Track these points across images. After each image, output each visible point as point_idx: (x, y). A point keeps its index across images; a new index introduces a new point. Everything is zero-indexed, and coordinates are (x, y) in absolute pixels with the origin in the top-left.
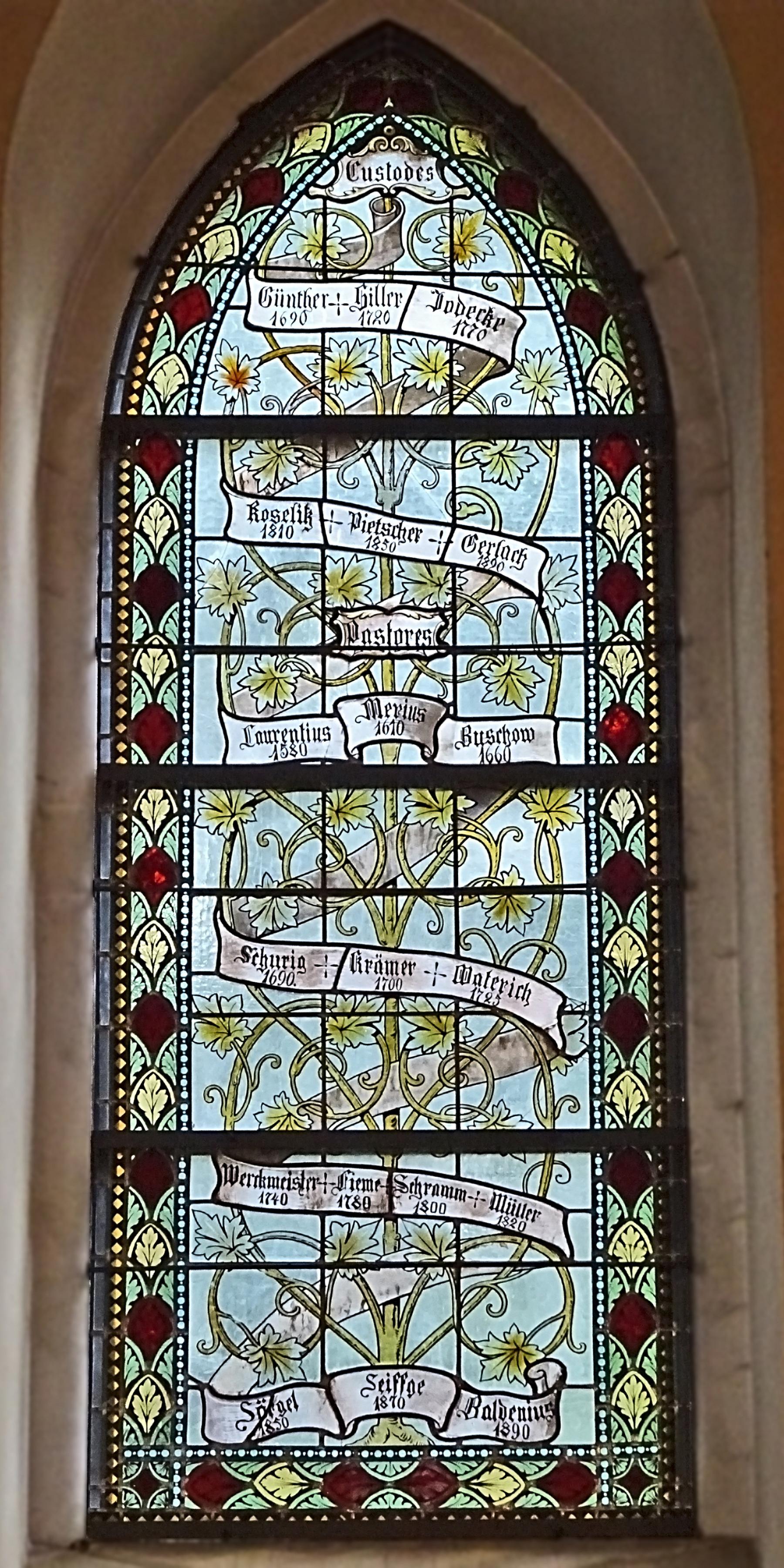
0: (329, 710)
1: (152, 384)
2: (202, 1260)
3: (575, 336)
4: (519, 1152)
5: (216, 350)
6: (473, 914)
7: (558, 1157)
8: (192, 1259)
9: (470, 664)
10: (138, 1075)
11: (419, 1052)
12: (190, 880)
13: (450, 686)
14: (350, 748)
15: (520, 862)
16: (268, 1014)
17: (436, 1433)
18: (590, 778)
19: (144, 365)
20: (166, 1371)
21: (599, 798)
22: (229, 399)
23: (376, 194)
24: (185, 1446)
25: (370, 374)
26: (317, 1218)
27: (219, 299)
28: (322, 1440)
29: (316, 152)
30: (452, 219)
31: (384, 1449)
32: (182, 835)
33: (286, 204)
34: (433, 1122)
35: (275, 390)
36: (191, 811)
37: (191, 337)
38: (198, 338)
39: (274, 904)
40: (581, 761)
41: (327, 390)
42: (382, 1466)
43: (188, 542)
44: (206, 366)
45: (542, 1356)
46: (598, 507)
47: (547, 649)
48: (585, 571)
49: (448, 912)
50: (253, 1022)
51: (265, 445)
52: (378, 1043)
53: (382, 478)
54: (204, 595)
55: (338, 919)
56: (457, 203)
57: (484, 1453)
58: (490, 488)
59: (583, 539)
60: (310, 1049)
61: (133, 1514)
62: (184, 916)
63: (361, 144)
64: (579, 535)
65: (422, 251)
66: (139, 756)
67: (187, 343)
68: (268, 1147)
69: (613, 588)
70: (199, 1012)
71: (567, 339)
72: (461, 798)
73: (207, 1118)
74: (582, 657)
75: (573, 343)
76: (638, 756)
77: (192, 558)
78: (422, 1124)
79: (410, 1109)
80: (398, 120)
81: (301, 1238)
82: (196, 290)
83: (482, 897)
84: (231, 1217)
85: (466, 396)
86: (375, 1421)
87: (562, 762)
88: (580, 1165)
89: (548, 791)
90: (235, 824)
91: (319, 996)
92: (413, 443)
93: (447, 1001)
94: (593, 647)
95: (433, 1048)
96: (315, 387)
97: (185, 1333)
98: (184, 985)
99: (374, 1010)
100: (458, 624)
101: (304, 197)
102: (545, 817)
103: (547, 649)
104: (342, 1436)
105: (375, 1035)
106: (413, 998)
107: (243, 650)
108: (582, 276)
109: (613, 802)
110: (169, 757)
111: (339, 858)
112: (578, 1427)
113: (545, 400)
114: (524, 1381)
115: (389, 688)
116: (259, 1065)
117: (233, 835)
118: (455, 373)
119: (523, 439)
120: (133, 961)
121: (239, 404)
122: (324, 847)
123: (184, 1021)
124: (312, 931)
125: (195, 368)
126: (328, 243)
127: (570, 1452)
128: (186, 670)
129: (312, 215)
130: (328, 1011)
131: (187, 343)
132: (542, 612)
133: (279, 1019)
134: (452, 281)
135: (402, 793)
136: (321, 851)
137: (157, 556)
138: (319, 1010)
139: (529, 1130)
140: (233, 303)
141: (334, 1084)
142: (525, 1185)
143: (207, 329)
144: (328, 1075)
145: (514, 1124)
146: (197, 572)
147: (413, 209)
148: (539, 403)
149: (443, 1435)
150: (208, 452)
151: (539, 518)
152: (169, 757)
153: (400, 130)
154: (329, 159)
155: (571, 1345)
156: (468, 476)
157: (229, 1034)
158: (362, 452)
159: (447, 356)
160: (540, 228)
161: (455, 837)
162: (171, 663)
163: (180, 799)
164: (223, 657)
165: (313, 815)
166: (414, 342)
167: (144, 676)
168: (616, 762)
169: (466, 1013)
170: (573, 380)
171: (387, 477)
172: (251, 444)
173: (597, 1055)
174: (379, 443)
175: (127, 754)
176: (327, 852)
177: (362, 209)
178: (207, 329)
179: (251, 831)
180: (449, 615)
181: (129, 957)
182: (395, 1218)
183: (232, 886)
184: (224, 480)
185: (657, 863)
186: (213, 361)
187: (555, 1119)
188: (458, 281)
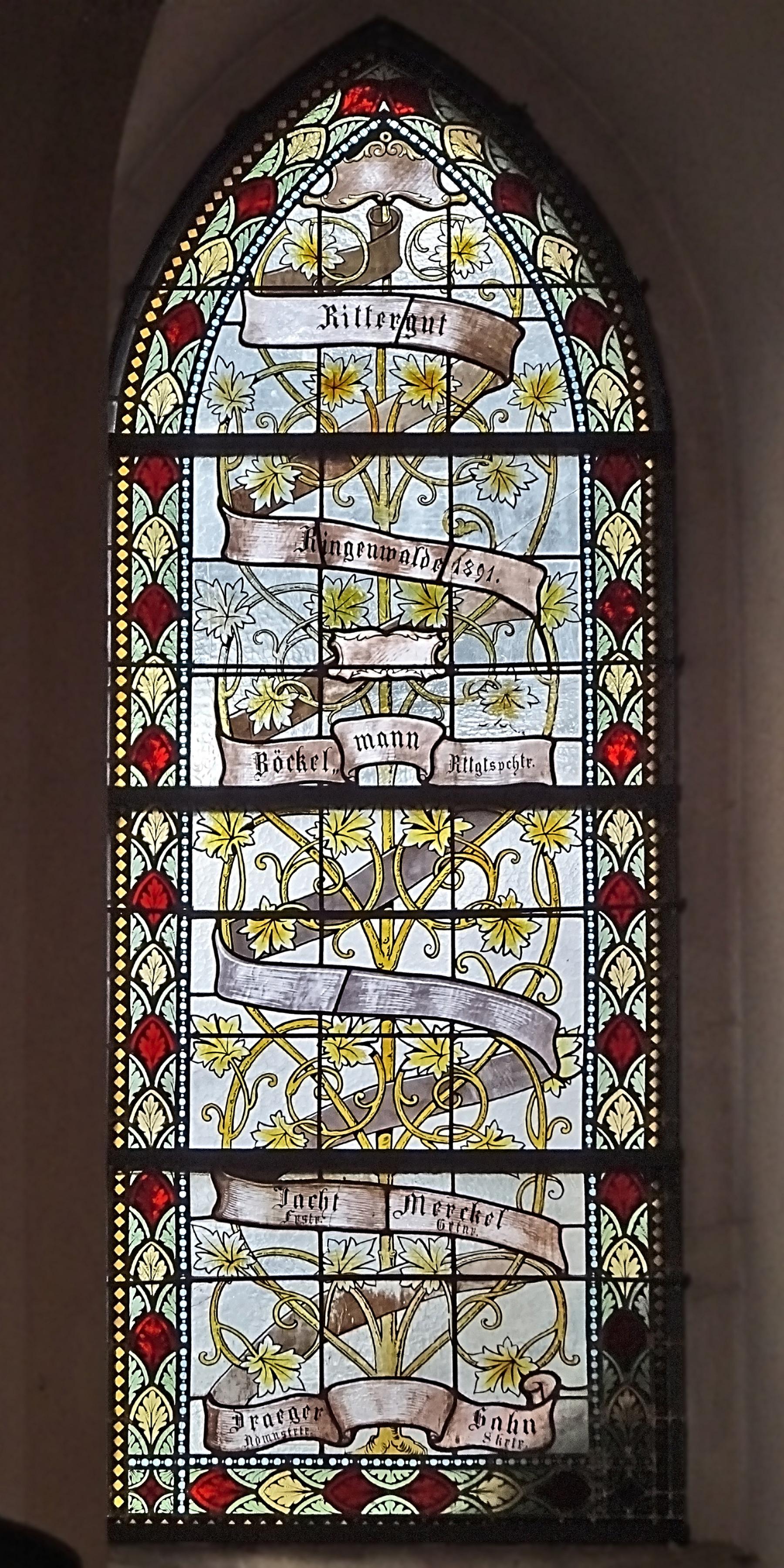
0: (326, 732)
1: (146, 404)
3: (575, 346)
5: (211, 368)
6: (469, 938)
8: (195, 1273)
10: (137, 1096)
13: (447, 708)
14: (346, 772)
15: (517, 884)
16: (267, 1035)
18: (588, 799)
22: (222, 419)
23: (371, 203)
26: (316, 1234)
27: (213, 316)
29: (310, 160)
31: (383, 1457)
32: (180, 640)
33: (280, 213)
34: (426, 1142)
35: (274, 408)
36: (189, 836)
37: (185, 356)
38: (191, 356)
40: (579, 783)
42: (381, 1473)
43: (185, 563)
44: (200, 385)
45: (534, 1368)
47: (545, 668)
48: (584, 590)
49: (445, 936)
50: (250, 1042)
52: (375, 1063)
54: (203, 619)
55: (335, 943)
57: (482, 1462)
59: (582, 557)
60: (305, 1069)
61: (140, 1518)
62: (185, 942)
63: (355, 150)
64: (578, 553)
66: (138, 778)
67: (180, 361)
68: (261, 1166)
69: (612, 607)
70: (197, 1032)
71: (566, 351)
73: (204, 1136)
74: (580, 676)
75: (572, 355)
76: (635, 777)
77: (190, 579)
78: (415, 1144)
79: (403, 1129)
80: (394, 124)
81: (297, 1253)
82: (189, 308)
83: (479, 920)
84: (230, 1233)
86: (374, 1431)
89: (546, 812)
90: (234, 847)
91: (316, 1017)
93: (442, 1024)
94: (592, 668)
95: (428, 1069)
96: (312, 848)
97: (188, 1346)
98: (183, 1006)
99: (369, 1032)
101: (298, 206)
102: (544, 840)
103: (545, 668)
105: (372, 1055)
106: (408, 1020)
108: (583, 286)
109: (145, 823)
110: (168, 779)
111: (337, 881)
114: (518, 1392)
116: (256, 1086)
117: (230, 639)
118: (452, 389)
120: (133, 984)
121: (233, 423)
122: (322, 869)
123: (183, 1041)
124: (308, 952)
125: (189, 388)
129: (308, 223)
130: (324, 1032)
131: (180, 361)
134: (449, 294)
135: (399, 815)
136: (318, 875)
138: (316, 1031)
139: (522, 1150)
140: (227, 319)
141: (330, 1102)
142: (519, 1201)
143: (201, 347)
144: (323, 1092)
145: (508, 1145)
146: (195, 595)
147: (412, 216)
148: (537, 419)
150: (204, 471)
151: (536, 541)
152: (168, 779)
153: (396, 135)
154: (324, 166)
155: (564, 1359)
156: (466, 494)
159: (444, 370)
160: (538, 233)
161: (452, 859)
163: (179, 824)
165: (311, 839)
166: (411, 358)
167: (610, 695)
168: (613, 783)
169: (460, 1035)
170: (571, 393)
174: (377, 459)
175: (126, 777)
176: (325, 874)
177: (359, 217)
178: (201, 347)
180: (446, 635)
181: (129, 836)
182: (390, 1233)
183: (230, 908)
184: (220, 498)
185: (657, 887)
186: (208, 378)
187: (547, 1140)
188: (455, 294)
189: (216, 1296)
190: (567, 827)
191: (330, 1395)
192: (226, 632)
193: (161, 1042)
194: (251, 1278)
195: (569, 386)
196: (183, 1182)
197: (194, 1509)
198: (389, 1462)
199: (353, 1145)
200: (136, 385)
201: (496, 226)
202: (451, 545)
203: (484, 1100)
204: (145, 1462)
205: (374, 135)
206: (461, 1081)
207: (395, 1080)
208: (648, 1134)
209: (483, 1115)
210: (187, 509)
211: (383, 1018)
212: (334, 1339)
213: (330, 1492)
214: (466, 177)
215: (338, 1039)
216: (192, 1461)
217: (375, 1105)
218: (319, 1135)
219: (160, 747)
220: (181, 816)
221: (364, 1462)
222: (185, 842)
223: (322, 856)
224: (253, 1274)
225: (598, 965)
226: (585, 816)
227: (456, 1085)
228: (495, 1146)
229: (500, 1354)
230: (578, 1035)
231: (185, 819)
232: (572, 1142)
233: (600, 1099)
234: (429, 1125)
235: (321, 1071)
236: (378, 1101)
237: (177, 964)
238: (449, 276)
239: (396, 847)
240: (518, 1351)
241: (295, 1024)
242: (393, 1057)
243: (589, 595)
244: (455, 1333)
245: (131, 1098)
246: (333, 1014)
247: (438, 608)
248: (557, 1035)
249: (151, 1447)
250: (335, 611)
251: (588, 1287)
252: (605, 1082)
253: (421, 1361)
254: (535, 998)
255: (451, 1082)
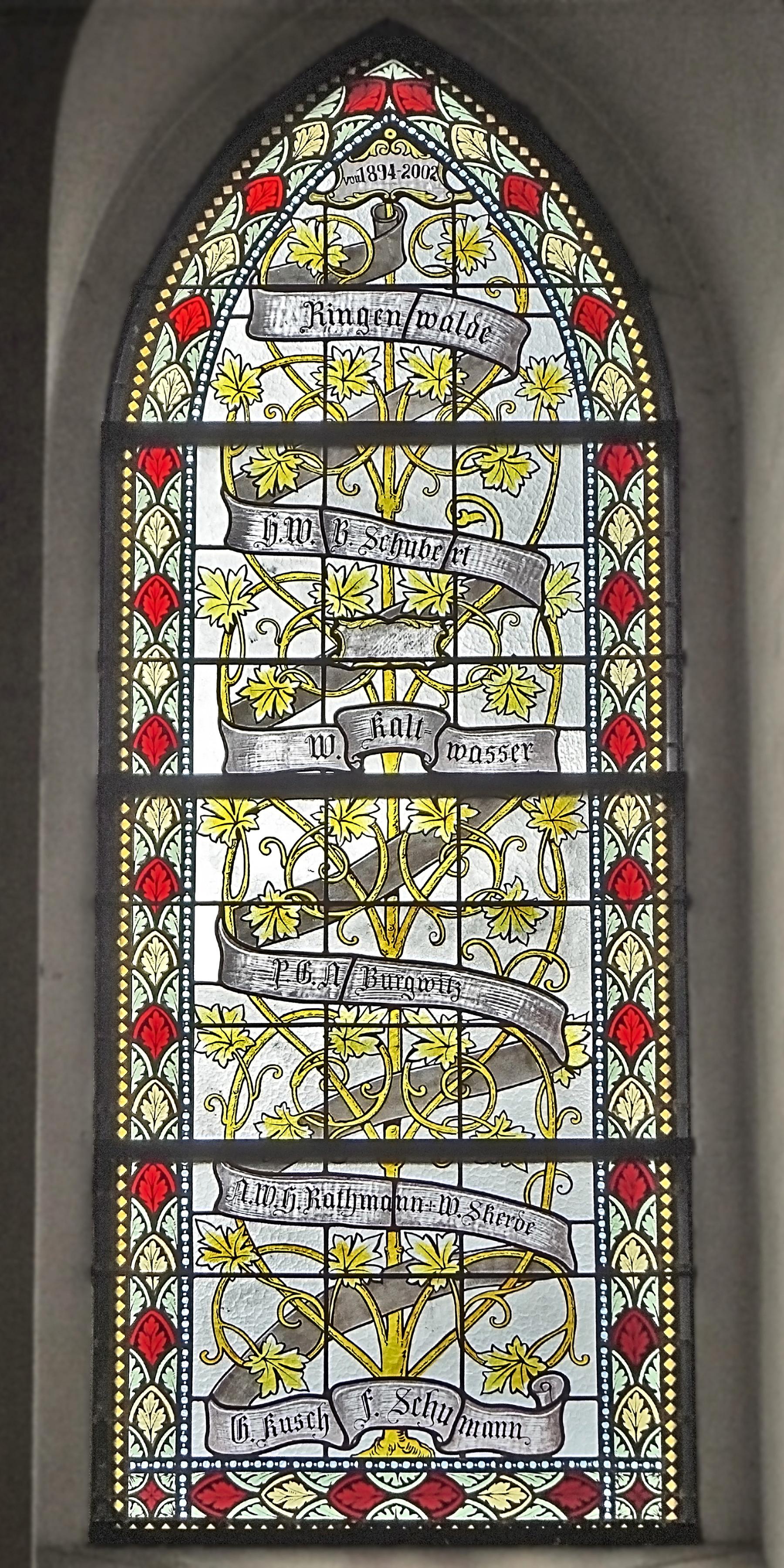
0: (330, 720)
2: (206, 1270)
4: (520, 1162)
5: (219, 360)
6: (475, 925)
7: (559, 1166)
8: (197, 1270)
9: (470, 674)
11: (422, 1063)
12: (192, 892)
17: (439, 1446)
19: (146, 375)
20: (170, 1382)
21: (602, 809)
23: (378, 200)
24: (189, 1459)
25: (373, 382)
27: (222, 306)
28: (326, 1452)
30: (454, 224)
31: (388, 1460)
36: (193, 822)
39: (276, 915)
41: (329, 398)
42: (387, 1476)
45: (543, 1368)
46: (601, 513)
48: (587, 579)
50: (255, 1032)
51: (265, 451)
53: (382, 485)
54: (206, 607)
56: (459, 208)
58: (490, 495)
59: (585, 546)
60: (312, 1061)
65: (425, 258)
66: (139, 767)
72: (464, 807)
73: (207, 1127)
78: (423, 1134)
79: (411, 1120)
84: (234, 1228)
85: (469, 404)
86: (379, 1433)
87: (563, 770)
88: (582, 1173)
90: (238, 830)
91: (322, 1006)
92: (414, 449)
93: (450, 1013)
94: (595, 663)
96: (318, 395)
98: (186, 994)
99: (377, 1021)
100: (460, 634)
102: (550, 826)
104: (346, 1446)
105: (378, 1046)
107: (242, 662)
110: (171, 767)
112: (582, 1441)
113: (549, 407)
115: (389, 699)
117: (232, 628)
118: (459, 381)
119: (526, 443)
121: (241, 411)
122: (327, 857)
123: (187, 1030)
124: (312, 942)
126: (330, 251)
127: (572, 1464)
128: (186, 1116)
129: (313, 222)
132: (544, 620)
133: (281, 1029)
135: (404, 802)
137: (158, 849)
140: (234, 312)
142: (527, 1192)
146: (197, 581)
147: (415, 213)
149: (446, 1449)
150: (208, 464)
151: (540, 527)
152: (171, 767)
155: (573, 1360)
156: (468, 484)
157: (231, 1045)
158: (363, 458)
159: (450, 365)
161: (459, 846)
162: (173, 534)
163: (183, 811)
164: (223, 668)
165: (316, 824)
167: (147, 547)
171: (387, 483)
172: (252, 452)
173: (599, 1066)
174: (381, 449)
177: (363, 215)
179: (253, 839)
184: (224, 488)
186: (216, 370)
189: (219, 1292)
190: (573, 813)
191: (335, 1397)
192: (227, 620)
193: (164, 1030)
194: (253, 1275)
195: (575, 376)
196: (185, 1173)
197: (196, 1513)
198: (394, 1465)
199: (360, 1136)
200: (146, 375)
201: (500, 222)
202: (455, 533)
203: (493, 1092)
204: (145, 1465)
205: (379, 135)
206: (469, 1071)
207: (402, 1070)
208: (660, 1122)
209: (490, 1107)
210: (189, 495)
211: (391, 1008)
212: (340, 1337)
213: (333, 1496)
214: (472, 176)
215: (343, 1030)
216: (195, 1465)
217: (381, 1097)
218: (326, 1127)
219: (165, 737)
220: (185, 802)
221: (369, 1465)
222: (189, 827)
223: (326, 843)
224: (256, 1271)
225: (605, 953)
226: (591, 801)
227: (464, 1076)
228: (503, 1135)
229: (508, 1352)
230: (586, 1024)
231: (189, 805)
232: (584, 1131)
233: (611, 1087)
234: (438, 1116)
235: (326, 1065)
236: (385, 1091)
237: (180, 953)
238: (455, 275)
239: (402, 833)
240: (528, 1349)
241: (298, 1014)
242: (400, 1046)
243: (592, 584)
244: (463, 1333)
245: (134, 1087)
246: (340, 1002)
247: (442, 595)
248: (565, 1024)
249: (152, 1450)
250: (340, 598)
251: (598, 1284)
252: (615, 1071)
253: (429, 1359)
254: (541, 986)
255: (460, 1073)
